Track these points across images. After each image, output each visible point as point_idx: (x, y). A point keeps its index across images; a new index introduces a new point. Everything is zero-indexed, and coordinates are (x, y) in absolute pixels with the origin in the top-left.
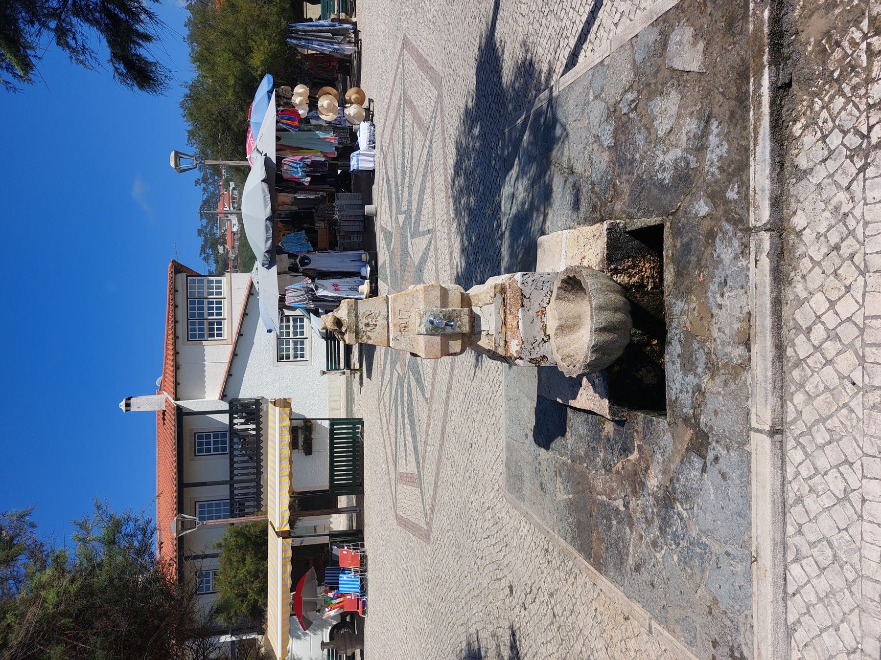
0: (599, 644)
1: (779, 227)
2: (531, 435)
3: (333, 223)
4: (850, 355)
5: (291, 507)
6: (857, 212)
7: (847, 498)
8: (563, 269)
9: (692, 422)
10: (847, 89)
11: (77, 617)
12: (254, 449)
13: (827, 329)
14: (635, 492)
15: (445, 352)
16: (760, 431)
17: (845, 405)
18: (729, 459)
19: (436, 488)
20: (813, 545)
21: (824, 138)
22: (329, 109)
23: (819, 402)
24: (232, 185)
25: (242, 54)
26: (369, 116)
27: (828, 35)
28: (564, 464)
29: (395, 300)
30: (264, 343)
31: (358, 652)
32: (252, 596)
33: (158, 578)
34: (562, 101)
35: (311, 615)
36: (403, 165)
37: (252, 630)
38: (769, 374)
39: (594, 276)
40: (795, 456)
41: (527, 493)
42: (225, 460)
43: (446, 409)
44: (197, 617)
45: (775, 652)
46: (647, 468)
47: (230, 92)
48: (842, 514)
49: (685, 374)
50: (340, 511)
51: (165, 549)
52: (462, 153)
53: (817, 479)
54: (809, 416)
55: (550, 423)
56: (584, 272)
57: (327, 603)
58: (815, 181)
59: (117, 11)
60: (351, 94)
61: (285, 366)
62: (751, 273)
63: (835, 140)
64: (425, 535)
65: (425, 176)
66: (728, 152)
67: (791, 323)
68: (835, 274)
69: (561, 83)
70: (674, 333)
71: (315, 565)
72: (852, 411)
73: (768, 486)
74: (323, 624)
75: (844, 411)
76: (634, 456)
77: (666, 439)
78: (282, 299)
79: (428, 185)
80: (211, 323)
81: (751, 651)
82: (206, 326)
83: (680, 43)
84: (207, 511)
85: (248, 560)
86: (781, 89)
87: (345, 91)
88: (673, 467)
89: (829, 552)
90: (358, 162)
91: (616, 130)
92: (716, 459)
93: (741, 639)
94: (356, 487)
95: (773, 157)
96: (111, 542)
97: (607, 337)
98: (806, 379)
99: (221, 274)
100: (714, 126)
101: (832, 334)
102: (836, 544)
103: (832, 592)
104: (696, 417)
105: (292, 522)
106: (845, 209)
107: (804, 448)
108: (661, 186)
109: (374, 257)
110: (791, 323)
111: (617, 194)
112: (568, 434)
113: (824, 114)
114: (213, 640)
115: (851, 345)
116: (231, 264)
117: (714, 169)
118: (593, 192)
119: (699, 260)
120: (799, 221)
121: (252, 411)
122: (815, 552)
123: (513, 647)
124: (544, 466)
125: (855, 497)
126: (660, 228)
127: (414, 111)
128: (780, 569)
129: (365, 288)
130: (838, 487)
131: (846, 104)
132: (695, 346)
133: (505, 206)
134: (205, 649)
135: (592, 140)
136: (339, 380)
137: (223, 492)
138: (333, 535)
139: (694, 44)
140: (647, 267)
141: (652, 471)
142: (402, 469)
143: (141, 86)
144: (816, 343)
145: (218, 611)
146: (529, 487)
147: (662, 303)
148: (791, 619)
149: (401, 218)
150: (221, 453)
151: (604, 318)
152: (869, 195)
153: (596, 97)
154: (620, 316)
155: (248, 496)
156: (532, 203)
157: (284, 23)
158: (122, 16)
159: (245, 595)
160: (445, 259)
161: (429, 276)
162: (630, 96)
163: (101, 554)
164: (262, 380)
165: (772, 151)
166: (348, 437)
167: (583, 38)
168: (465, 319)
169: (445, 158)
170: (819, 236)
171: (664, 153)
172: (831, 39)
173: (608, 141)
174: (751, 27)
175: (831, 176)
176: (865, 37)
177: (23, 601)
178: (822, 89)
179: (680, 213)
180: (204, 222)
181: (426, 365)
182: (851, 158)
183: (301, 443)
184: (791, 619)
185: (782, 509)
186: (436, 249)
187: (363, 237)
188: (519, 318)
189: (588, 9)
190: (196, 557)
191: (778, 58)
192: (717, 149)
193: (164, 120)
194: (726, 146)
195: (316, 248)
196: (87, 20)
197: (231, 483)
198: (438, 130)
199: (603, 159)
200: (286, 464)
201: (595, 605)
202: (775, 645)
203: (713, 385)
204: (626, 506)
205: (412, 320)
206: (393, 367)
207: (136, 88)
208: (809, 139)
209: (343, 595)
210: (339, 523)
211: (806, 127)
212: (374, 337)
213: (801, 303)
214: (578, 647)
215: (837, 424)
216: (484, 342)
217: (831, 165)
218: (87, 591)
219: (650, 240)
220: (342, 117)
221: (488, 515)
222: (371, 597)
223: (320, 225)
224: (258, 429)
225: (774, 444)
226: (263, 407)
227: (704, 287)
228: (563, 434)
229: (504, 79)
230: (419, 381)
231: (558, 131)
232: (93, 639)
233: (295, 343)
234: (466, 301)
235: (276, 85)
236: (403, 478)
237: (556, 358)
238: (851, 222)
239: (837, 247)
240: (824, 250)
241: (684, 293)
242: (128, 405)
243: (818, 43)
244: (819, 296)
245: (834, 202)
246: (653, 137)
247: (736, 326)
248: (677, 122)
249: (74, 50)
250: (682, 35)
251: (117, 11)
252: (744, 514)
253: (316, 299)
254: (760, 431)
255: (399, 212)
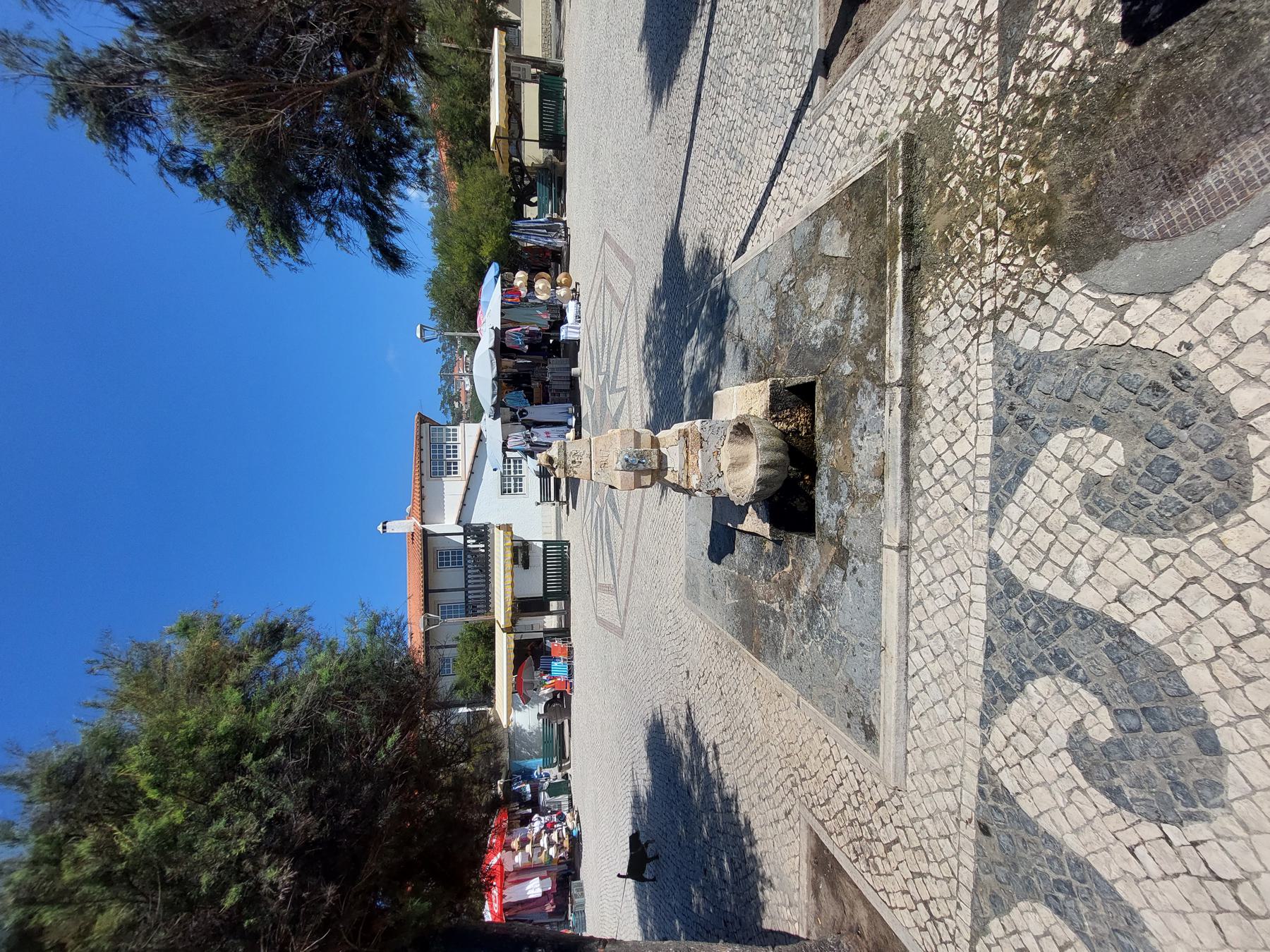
0: (757, 716)
1: (909, 383)
2: (706, 553)
3: (545, 384)
4: (964, 486)
5: (513, 610)
6: (972, 371)
7: (958, 600)
8: (734, 417)
9: (836, 541)
10: (965, 272)
11: (347, 691)
12: (483, 564)
13: (946, 466)
14: (788, 597)
15: (638, 485)
16: (890, 547)
17: (959, 526)
18: (865, 569)
19: (628, 595)
20: (929, 637)
21: (946, 311)
22: (543, 291)
23: (937, 523)
24: (466, 353)
25: (474, 247)
26: (576, 296)
27: (949, 227)
28: (733, 575)
29: (596, 441)
30: (490, 479)
31: (566, 721)
32: (483, 677)
33: (409, 661)
34: (734, 280)
35: (530, 693)
36: (603, 336)
37: (483, 703)
38: (899, 501)
39: (760, 423)
40: (918, 567)
41: (702, 598)
42: (460, 572)
43: (638, 532)
44: (440, 691)
45: (896, 720)
46: (799, 578)
47: (465, 277)
48: (954, 613)
49: (831, 503)
50: (551, 613)
51: (415, 640)
52: (651, 325)
53: (935, 585)
54: (929, 535)
55: (722, 542)
56: (752, 420)
57: (542, 684)
58: (938, 346)
59: (375, 208)
60: (561, 278)
61: (507, 497)
62: (886, 420)
63: (955, 312)
64: (620, 633)
65: (621, 343)
66: (869, 322)
67: (917, 461)
68: (953, 420)
69: (732, 267)
70: (823, 470)
71: (531, 654)
72: (964, 531)
73: (896, 591)
74: (539, 700)
75: (958, 531)
76: (788, 569)
77: (815, 555)
78: (504, 444)
79: (624, 351)
80: (449, 464)
81: (878, 719)
82: (445, 466)
83: (830, 234)
84: (448, 611)
85: (480, 650)
86: (912, 272)
87: (557, 275)
88: (819, 576)
89: (942, 643)
90: (566, 333)
91: (777, 305)
92: (855, 570)
93: (870, 711)
94: (564, 595)
95: (904, 327)
96: (373, 632)
97: (770, 472)
98: (927, 506)
99: (457, 424)
100: (857, 302)
101: (950, 469)
102: (948, 636)
103: (943, 674)
104: (839, 537)
105: (514, 622)
106: (962, 369)
107: (925, 560)
108: (814, 350)
109: (579, 409)
110: (917, 461)
111: (778, 357)
112: (736, 552)
113: (947, 291)
114: (454, 711)
115: (965, 478)
116: (464, 416)
117: (857, 336)
118: (759, 355)
119: (844, 410)
120: (925, 378)
121: (482, 533)
122: (931, 642)
123: (689, 718)
124: (716, 578)
125: (964, 599)
126: (813, 384)
127: (612, 291)
128: (903, 656)
129: (571, 435)
130: (951, 591)
131: (964, 283)
132: (840, 479)
133: (687, 366)
134: (447, 717)
135: (758, 313)
136: (550, 509)
137: (460, 597)
138: (546, 632)
139: (842, 235)
140: (802, 417)
141: (803, 581)
142: (600, 581)
143: (394, 269)
144: (937, 477)
145: (457, 688)
146: (703, 594)
147: (813, 446)
148: (910, 696)
149: (601, 378)
150: (458, 565)
151: (767, 457)
152: (982, 357)
153: (762, 278)
154: (780, 455)
155: (479, 601)
156: (708, 364)
157: (507, 220)
158: (379, 212)
159: (478, 677)
160: (637, 411)
161: (624, 423)
162: (789, 278)
163: (365, 641)
164: (491, 508)
165: (904, 321)
166: (558, 555)
167: (751, 230)
168: (655, 458)
169: (637, 330)
170: (941, 390)
171: (817, 324)
172: (952, 231)
173: (771, 313)
174: (888, 221)
175: (951, 341)
176: (979, 229)
177: (304, 677)
178: (944, 271)
179: (829, 372)
180: (444, 382)
181: (620, 496)
182: (967, 327)
183: (520, 559)
184: (910, 696)
185: (906, 609)
186: (630, 403)
187: (571, 392)
188: (698, 457)
189: (755, 207)
190: (438, 647)
191: (910, 246)
192: (859, 320)
193: (411, 296)
194: (867, 317)
195: (531, 402)
196: (351, 215)
197: (466, 590)
198: (632, 307)
199: (767, 329)
200: (509, 575)
201: (754, 685)
202: (897, 715)
203: (853, 511)
204: (781, 608)
205: (610, 458)
206: (594, 500)
207: (389, 270)
208: (934, 312)
209: (554, 678)
210: (551, 622)
211: (931, 302)
212: (580, 472)
213: (925, 444)
214: (740, 718)
215: (952, 541)
216: (669, 477)
217: (952, 333)
218: (353, 670)
219: (805, 393)
220: (554, 297)
221: (670, 616)
222: (576, 680)
223: (535, 385)
224: (486, 548)
225: (901, 557)
226: (490, 530)
227: (847, 432)
228: (732, 552)
229: (686, 265)
230: (614, 511)
231: (730, 306)
232: (360, 707)
233: (515, 480)
234: (655, 443)
235: (501, 271)
236: (602, 588)
237: (728, 490)
238: (967, 379)
239: (955, 400)
240: (945, 402)
241: (832, 437)
242: (384, 528)
243: (942, 234)
244: (940, 439)
245: (953, 363)
246: (807, 310)
247: (873, 463)
248: (827, 298)
249: (339, 240)
250: (832, 227)
251: (375, 208)
252: (875, 613)
253: (532, 445)
254: (890, 547)
255: (599, 373)
